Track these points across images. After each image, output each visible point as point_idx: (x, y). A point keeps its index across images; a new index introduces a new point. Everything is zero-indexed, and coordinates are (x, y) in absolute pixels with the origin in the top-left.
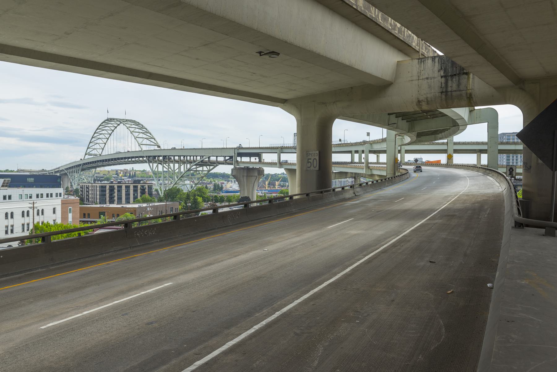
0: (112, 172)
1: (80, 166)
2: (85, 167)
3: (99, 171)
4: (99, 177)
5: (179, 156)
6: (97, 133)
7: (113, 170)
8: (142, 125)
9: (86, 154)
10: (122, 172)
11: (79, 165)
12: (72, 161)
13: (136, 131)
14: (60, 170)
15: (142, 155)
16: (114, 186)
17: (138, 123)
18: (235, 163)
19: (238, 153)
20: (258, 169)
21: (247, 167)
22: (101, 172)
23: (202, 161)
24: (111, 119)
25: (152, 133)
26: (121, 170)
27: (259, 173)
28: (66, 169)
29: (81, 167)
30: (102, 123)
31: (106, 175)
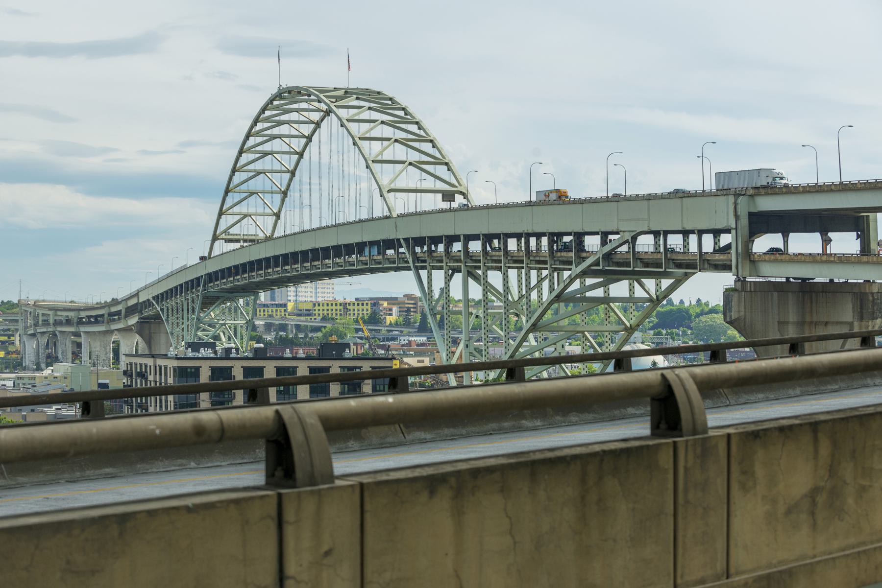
0: (356, 307)
1: (199, 285)
2: (214, 288)
3: (310, 307)
4: (306, 326)
5: (656, 234)
6: (249, 151)
7: (364, 299)
8: (403, 109)
9: (215, 238)
10: (395, 309)
11: (193, 284)
12: (177, 266)
13: (372, 136)
14: (141, 301)
15: (392, 236)
16: (230, 368)
17: (391, 99)
18: (740, 260)
19: (751, 215)
20: (856, 290)
21: (804, 280)
22: (317, 308)
23: (608, 257)
24: (290, 92)
25: (440, 143)
26: (392, 301)
27: (861, 308)
28: (157, 298)
29: (201, 288)
30: (263, 110)
31: (332, 319)
